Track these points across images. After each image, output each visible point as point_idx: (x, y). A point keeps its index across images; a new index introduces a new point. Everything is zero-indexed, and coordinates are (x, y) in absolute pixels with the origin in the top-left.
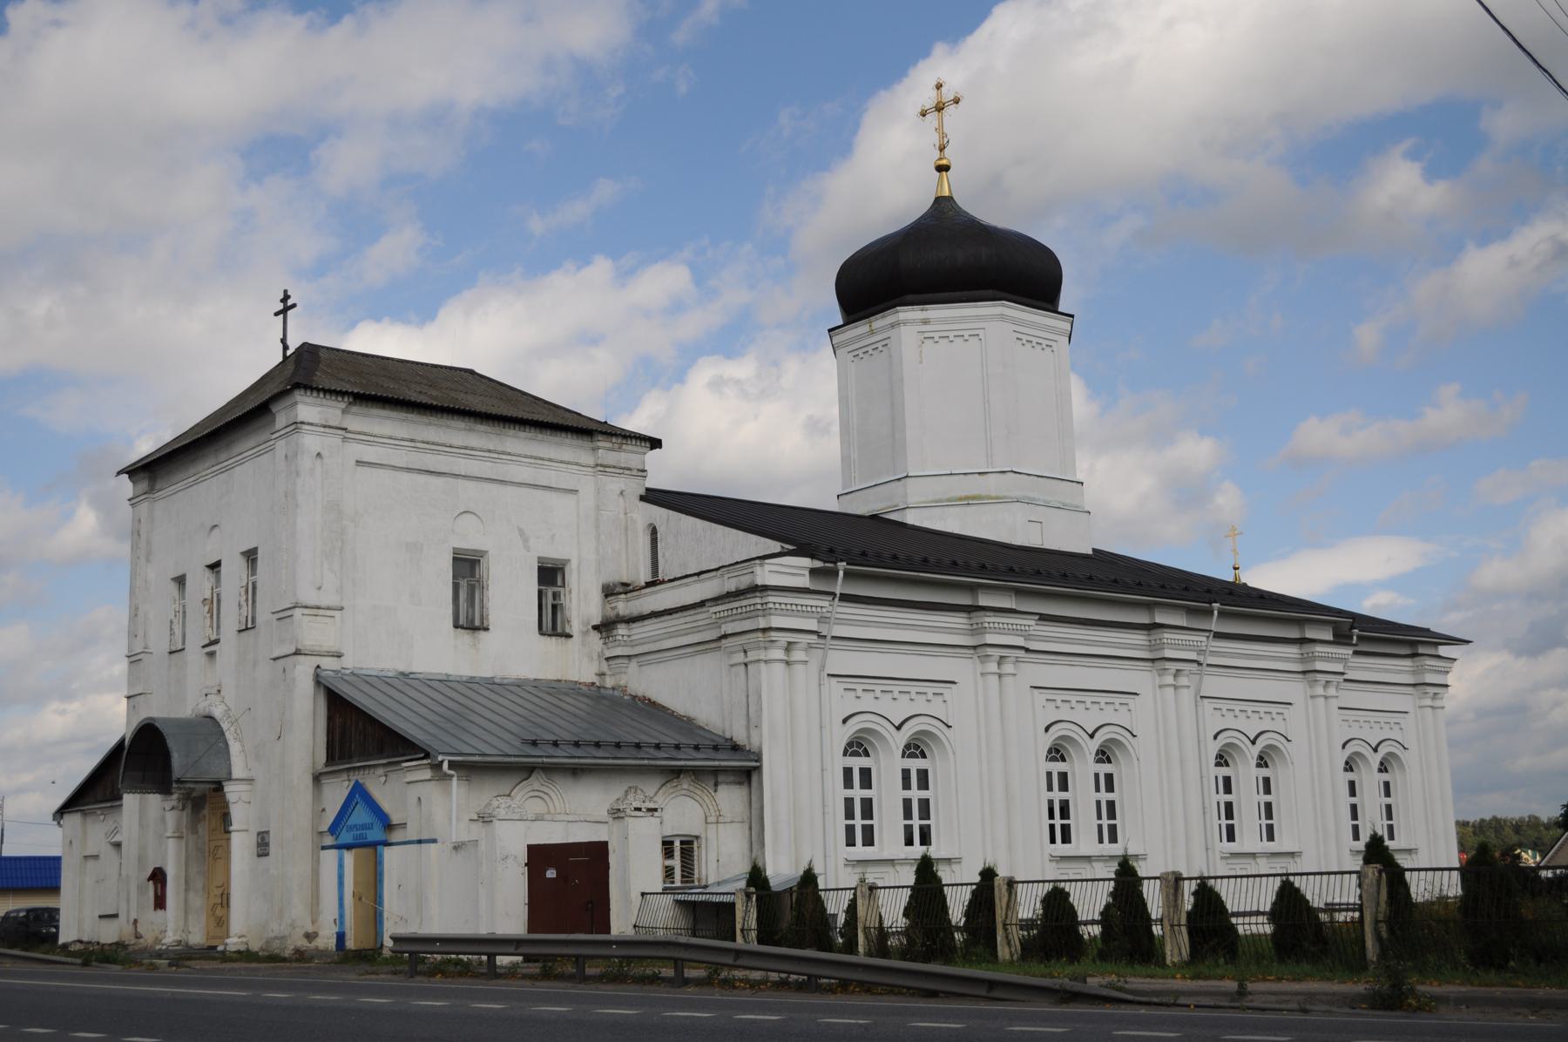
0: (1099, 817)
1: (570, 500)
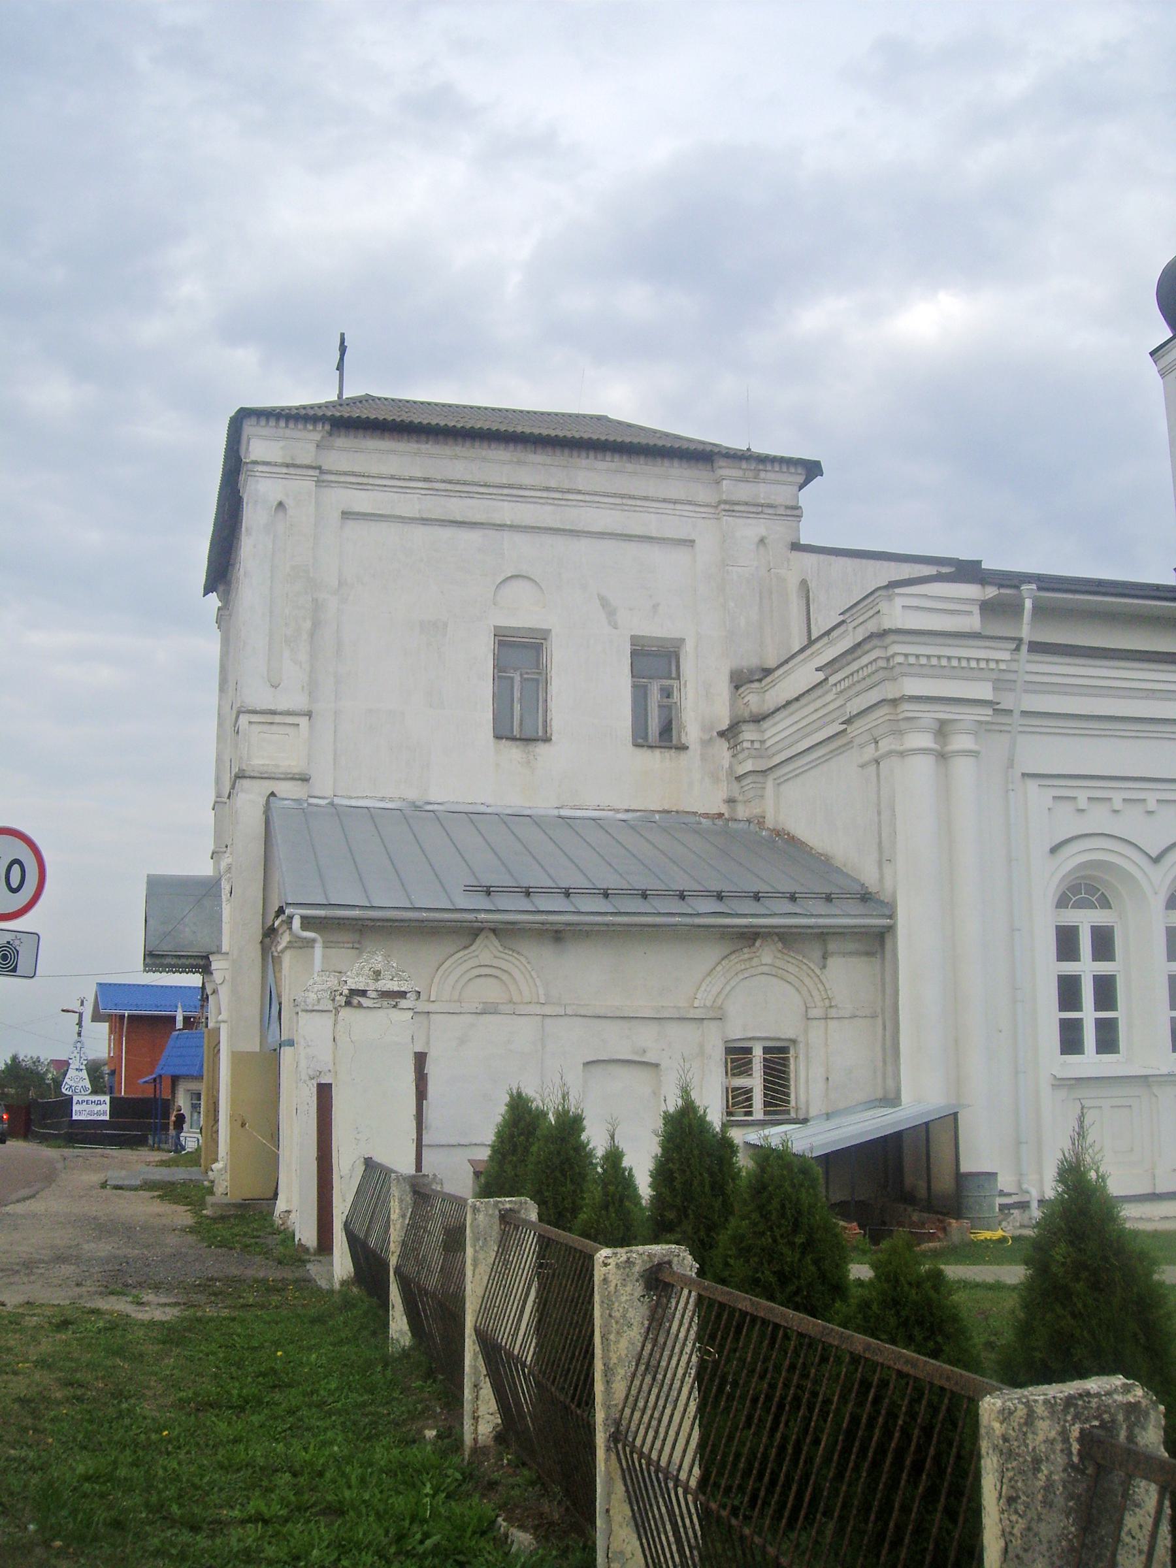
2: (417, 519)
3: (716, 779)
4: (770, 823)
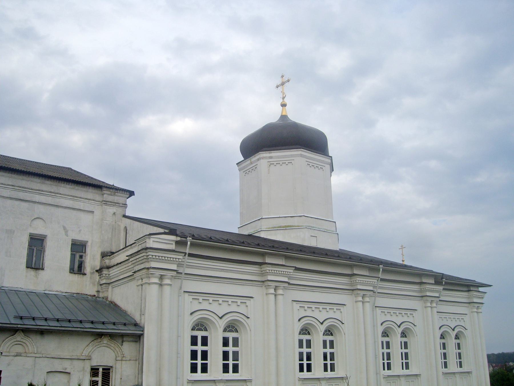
1: (89, 216)
2: (9, 198)
3: (94, 284)
4: (109, 299)
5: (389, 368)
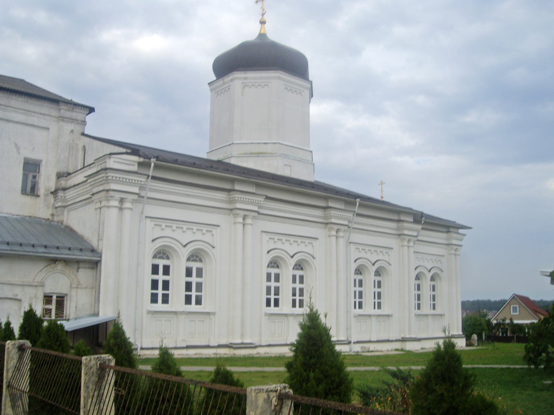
0: (355, 298)
1: (44, 133)
3: (48, 207)
4: (65, 223)
5: (360, 307)
